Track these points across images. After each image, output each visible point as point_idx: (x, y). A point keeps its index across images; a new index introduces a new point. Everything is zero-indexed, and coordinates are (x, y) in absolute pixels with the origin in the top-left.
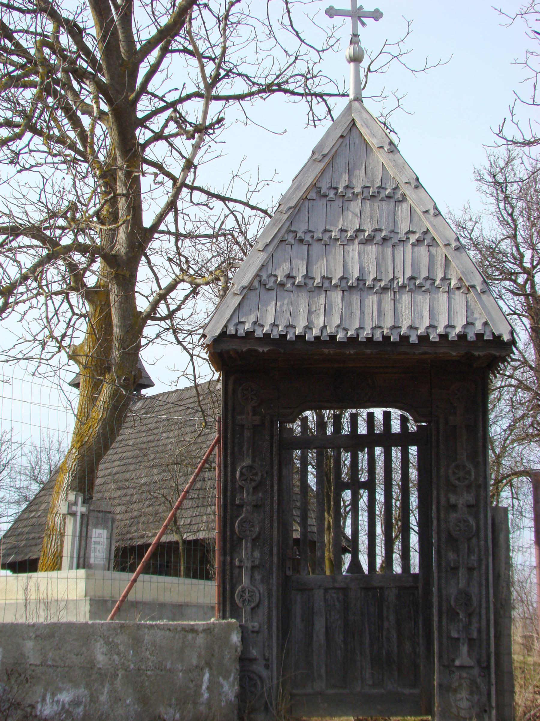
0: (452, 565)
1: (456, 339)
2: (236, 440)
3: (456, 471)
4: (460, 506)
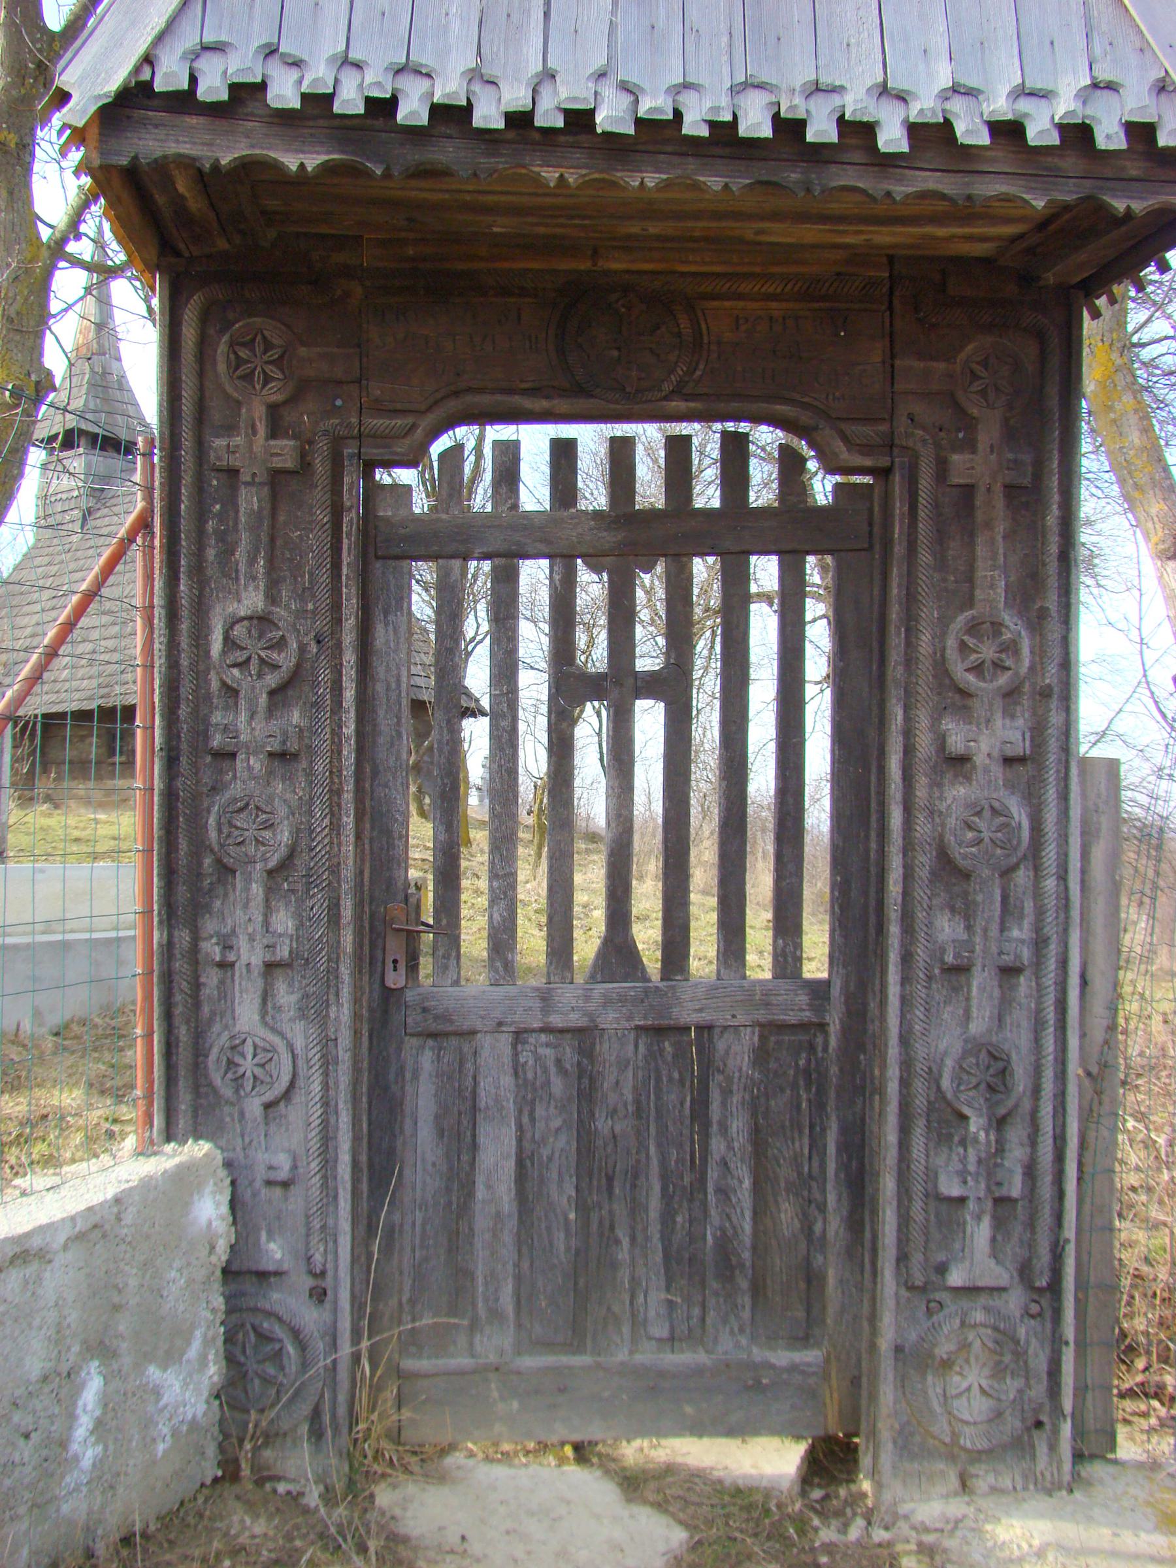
0: (949, 958)
1: (1054, 139)
2: (211, 525)
3: (971, 642)
4: (980, 759)
